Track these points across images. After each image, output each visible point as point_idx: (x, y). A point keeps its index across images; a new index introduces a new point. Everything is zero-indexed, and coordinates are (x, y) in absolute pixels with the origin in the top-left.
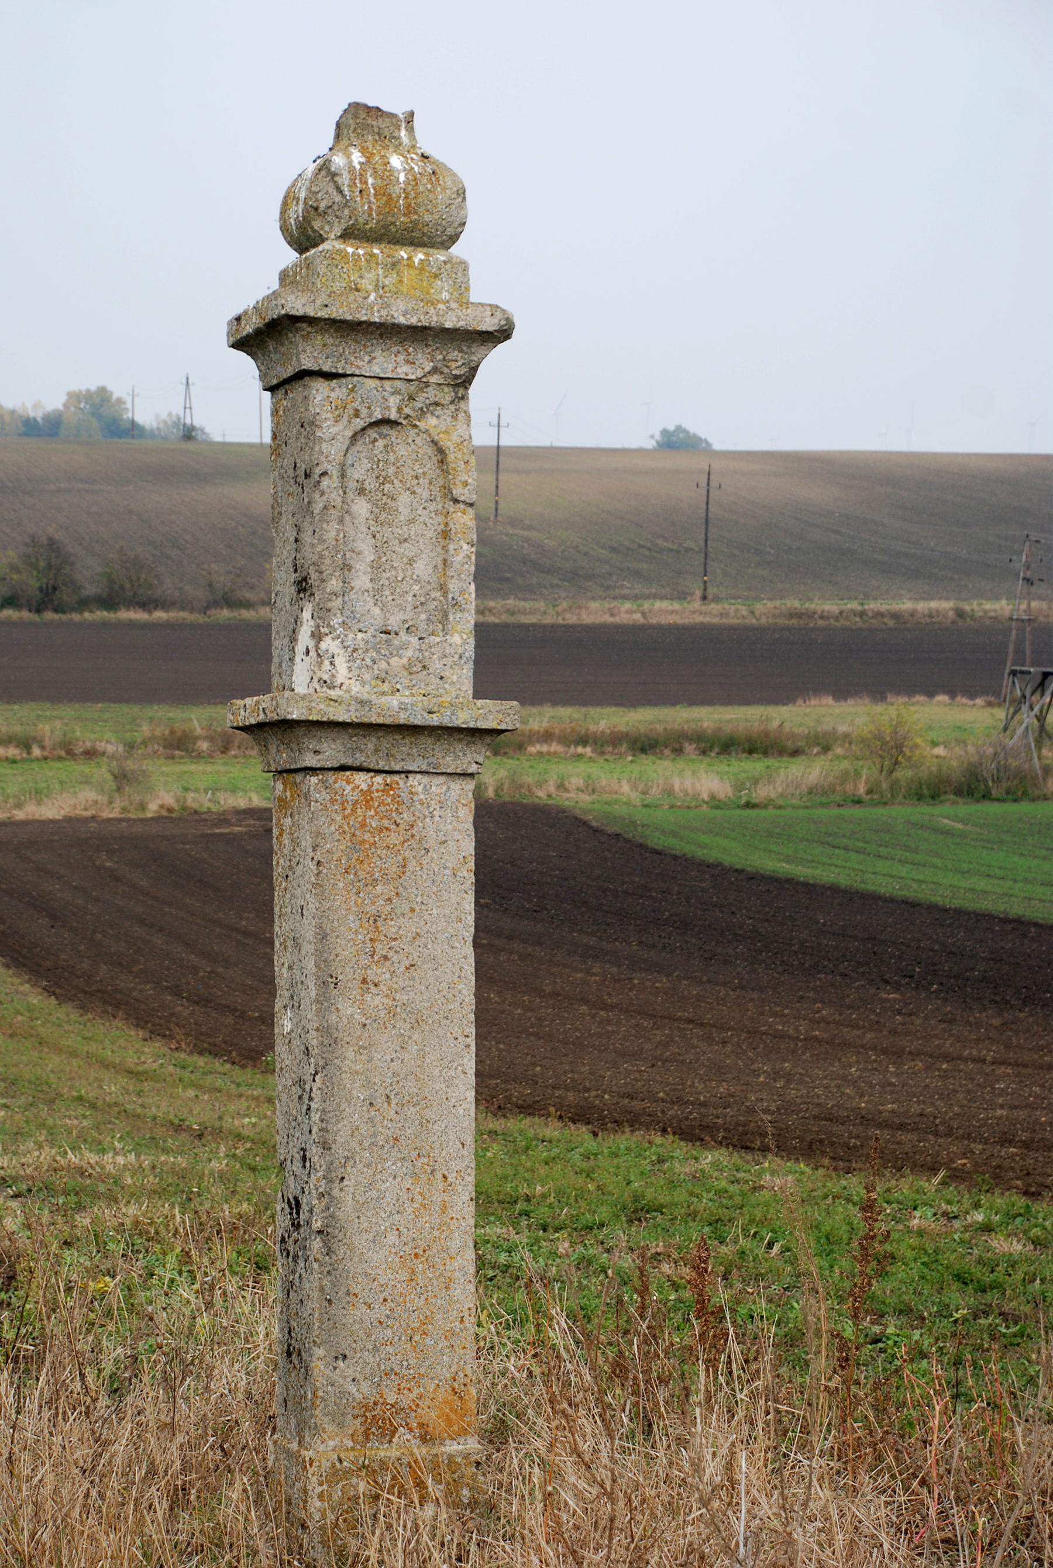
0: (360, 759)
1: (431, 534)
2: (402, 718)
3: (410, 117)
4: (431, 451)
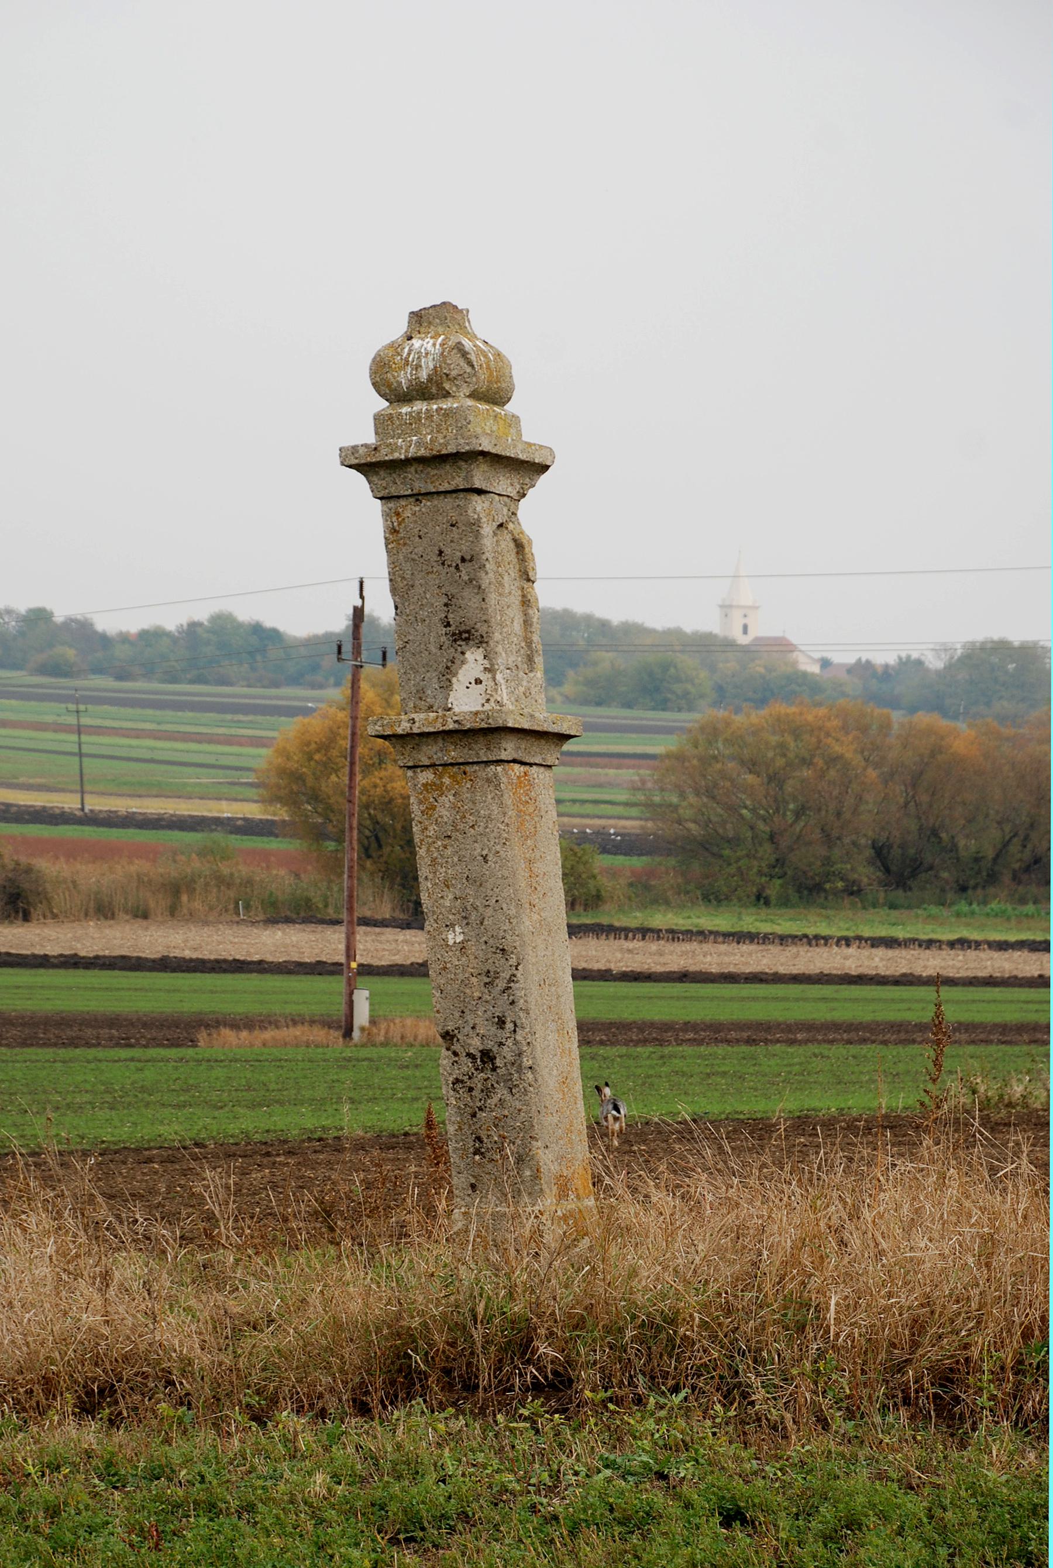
1: (517, 602)
3: (468, 311)
4: (512, 545)
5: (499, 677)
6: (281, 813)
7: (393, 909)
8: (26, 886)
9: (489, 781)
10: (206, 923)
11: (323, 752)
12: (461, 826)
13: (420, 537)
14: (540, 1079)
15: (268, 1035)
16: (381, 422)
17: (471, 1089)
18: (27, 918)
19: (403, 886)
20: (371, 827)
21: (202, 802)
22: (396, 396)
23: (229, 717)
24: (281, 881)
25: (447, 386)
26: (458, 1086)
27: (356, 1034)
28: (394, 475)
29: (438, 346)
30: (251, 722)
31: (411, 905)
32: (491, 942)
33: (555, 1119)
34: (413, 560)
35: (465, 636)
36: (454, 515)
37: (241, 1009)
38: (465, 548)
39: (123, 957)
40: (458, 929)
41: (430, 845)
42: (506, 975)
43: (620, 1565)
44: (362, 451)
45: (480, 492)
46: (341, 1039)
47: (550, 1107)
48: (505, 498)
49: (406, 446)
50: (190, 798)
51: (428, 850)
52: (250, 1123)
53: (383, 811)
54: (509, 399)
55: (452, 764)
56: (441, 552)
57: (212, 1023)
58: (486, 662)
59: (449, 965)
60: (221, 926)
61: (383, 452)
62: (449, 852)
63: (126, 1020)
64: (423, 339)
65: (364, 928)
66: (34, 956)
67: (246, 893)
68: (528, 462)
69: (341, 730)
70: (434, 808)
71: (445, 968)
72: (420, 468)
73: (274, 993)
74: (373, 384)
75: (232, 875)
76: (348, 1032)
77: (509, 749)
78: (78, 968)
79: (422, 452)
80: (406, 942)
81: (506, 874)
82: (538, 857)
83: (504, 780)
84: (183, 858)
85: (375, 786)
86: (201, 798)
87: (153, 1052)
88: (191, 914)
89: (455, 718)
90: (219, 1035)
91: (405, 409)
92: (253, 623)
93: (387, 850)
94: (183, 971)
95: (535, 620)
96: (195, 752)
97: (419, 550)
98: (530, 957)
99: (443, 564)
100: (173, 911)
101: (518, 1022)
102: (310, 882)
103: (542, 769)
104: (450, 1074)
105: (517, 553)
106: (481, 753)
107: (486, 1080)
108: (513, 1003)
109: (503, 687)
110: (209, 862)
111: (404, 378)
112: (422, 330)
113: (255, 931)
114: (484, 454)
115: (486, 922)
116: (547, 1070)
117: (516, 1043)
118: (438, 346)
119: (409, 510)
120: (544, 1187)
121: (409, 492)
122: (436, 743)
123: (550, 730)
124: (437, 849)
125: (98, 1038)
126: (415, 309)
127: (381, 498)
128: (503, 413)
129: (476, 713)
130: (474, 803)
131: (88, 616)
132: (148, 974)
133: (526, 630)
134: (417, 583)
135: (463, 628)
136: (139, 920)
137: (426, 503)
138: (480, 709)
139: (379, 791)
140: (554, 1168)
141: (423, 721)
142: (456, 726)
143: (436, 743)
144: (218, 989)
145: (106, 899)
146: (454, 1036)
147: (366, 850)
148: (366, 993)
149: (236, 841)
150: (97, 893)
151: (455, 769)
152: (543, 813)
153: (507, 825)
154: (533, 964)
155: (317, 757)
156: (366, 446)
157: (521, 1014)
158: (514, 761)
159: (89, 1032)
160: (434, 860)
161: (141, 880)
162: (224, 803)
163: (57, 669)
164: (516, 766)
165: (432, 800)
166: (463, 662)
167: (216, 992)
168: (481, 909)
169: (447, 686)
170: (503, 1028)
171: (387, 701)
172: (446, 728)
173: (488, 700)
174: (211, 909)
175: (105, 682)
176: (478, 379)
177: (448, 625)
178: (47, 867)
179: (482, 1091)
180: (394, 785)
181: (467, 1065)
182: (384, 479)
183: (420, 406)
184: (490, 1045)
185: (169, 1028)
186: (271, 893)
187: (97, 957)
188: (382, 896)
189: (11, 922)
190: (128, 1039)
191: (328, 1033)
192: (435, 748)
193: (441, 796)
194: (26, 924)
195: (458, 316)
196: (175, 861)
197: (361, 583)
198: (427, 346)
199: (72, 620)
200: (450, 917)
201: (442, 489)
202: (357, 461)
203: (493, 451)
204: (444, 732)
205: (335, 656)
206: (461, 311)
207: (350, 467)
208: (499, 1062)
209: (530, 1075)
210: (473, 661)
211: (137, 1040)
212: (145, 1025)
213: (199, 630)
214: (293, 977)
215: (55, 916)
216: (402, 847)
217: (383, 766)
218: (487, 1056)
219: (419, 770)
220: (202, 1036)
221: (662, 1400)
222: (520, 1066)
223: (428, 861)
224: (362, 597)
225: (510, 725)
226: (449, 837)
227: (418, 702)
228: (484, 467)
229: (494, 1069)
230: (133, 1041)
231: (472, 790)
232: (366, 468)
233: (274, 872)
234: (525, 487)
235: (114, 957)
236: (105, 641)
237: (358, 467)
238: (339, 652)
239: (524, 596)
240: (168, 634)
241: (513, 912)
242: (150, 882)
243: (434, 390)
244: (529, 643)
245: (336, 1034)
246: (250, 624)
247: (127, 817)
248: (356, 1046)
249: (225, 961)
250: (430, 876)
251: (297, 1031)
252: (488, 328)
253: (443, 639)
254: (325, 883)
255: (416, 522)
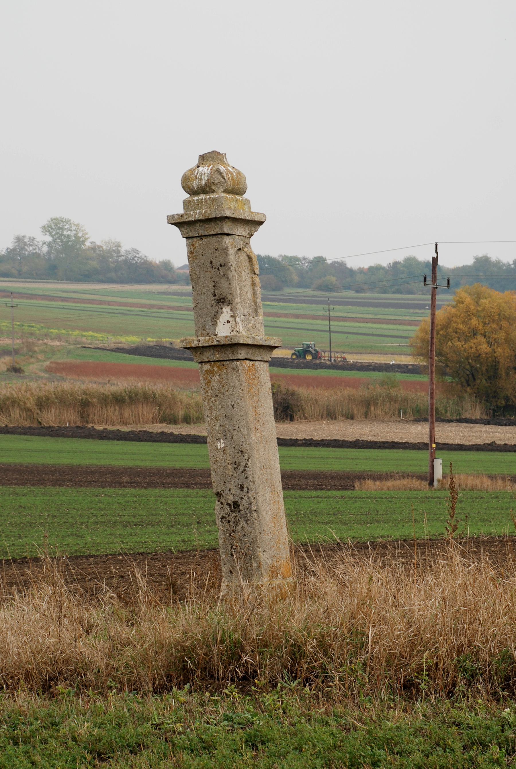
0: (248, 356)
1: (249, 284)
2: (261, 343)
3: (225, 154)
4: (246, 258)
5: (238, 319)
6: (422, 362)
7: (482, 414)
8: (292, 402)
9: (234, 369)
10: (383, 422)
11: (444, 330)
12: (222, 391)
13: (202, 255)
14: (261, 517)
15: (390, 483)
16: (187, 204)
17: (229, 522)
18: (292, 419)
19: (487, 401)
20: (470, 370)
21: (392, 356)
22: (193, 192)
23: (411, 311)
24: (422, 398)
25: (213, 187)
26: (223, 520)
27: (436, 483)
28: (191, 228)
29: (209, 170)
30: (422, 313)
31: (491, 411)
32: (236, 447)
33: (270, 537)
34: (200, 266)
35: (222, 301)
36: (217, 245)
37: (385, 469)
38: (221, 260)
39: (335, 440)
40: (222, 441)
41: (209, 400)
42: (243, 464)
43: (90, 767)
44: (176, 217)
45: (228, 235)
46: (428, 486)
47: (267, 531)
48: (242, 237)
49: (195, 215)
50: (387, 354)
51: (208, 403)
52: (365, 533)
53: (476, 361)
54: (245, 192)
55: (218, 361)
56: (211, 262)
57: (361, 477)
58: (231, 312)
59: (218, 459)
60: (390, 423)
61: (185, 217)
62: (217, 403)
63: (324, 475)
64: (203, 167)
65: (465, 424)
66: (291, 440)
67: (404, 405)
68: (251, 220)
69: (453, 318)
70: (210, 382)
71: (216, 460)
72: (201, 224)
73: (407, 460)
74: (183, 187)
75: (397, 395)
76: (431, 483)
77: (242, 354)
78: (312, 446)
79: (201, 217)
80: (486, 431)
81: (242, 414)
82: (260, 405)
83: (241, 368)
84: (372, 387)
85: (471, 348)
86: (393, 354)
87: (329, 493)
88: (375, 417)
89: (217, 339)
90: (365, 483)
91: (196, 198)
92: (426, 261)
93: (478, 381)
94: (365, 448)
95: (258, 292)
96: (392, 329)
97: (202, 261)
98: (255, 454)
99: (212, 267)
100: (366, 415)
101: (249, 487)
102: (441, 400)
103: (262, 363)
104: (220, 514)
105: (249, 261)
106: (230, 355)
107: (235, 517)
108: (247, 478)
109: (240, 324)
110: (385, 389)
111: (195, 184)
112: (204, 163)
113: (408, 426)
114: (227, 217)
115: (234, 438)
116: (265, 512)
117: (249, 498)
118: (209, 170)
119: (198, 243)
120: (263, 572)
121: (197, 235)
122: (210, 351)
123: (264, 344)
124: (212, 402)
125: (307, 485)
126: (202, 154)
127: (186, 238)
128: (241, 198)
129: (226, 337)
130: (227, 379)
131: (343, 260)
132: (346, 449)
133: (254, 297)
134: (202, 276)
135: (221, 297)
136: (349, 420)
137: (205, 240)
138: (229, 334)
139: (473, 350)
140: (269, 562)
141: (204, 341)
142: (218, 343)
143: (210, 351)
144: (379, 458)
145: (332, 408)
146: (221, 494)
147: (467, 382)
148: (440, 461)
149: (399, 376)
150: (327, 406)
151: (219, 363)
152: (263, 384)
153: (243, 390)
154: (257, 458)
155: (441, 333)
156: (178, 215)
157: (251, 483)
158: (246, 359)
159: (303, 481)
160: (211, 407)
161: (351, 399)
162: (403, 356)
163: (327, 288)
164: (248, 362)
165: (209, 378)
166: (222, 313)
167: (377, 460)
168: (232, 431)
169: (215, 324)
170: (243, 491)
171: (477, 303)
172: (213, 344)
173: (233, 331)
174: (386, 414)
175: (351, 294)
176: (227, 184)
177: (215, 295)
178: (303, 392)
179: (234, 522)
180: (481, 347)
181: (227, 509)
182: (186, 229)
183: (202, 196)
184: (237, 499)
185: (344, 479)
186: (417, 405)
187: (322, 440)
188: (476, 406)
189: (284, 421)
190: (322, 485)
191: (421, 483)
192: (210, 354)
193: (213, 376)
194: (291, 423)
195: (220, 157)
196: (368, 389)
197: (436, 245)
198: (205, 170)
199: (335, 262)
200: (218, 435)
201: (211, 233)
202: (174, 222)
203: (233, 216)
204: (212, 346)
205: (423, 283)
206: (222, 154)
207: (172, 224)
208: (241, 508)
209: (255, 514)
210: (226, 312)
211: (326, 486)
212: (332, 478)
213: (399, 266)
214: (421, 452)
215: (306, 418)
216: (486, 380)
217: (476, 337)
218: (236, 505)
219: (203, 364)
220: (357, 484)
221: (285, 685)
222: (251, 509)
223: (208, 407)
224: (437, 252)
225: (241, 342)
226: (217, 396)
227: (203, 332)
228: (229, 223)
229: (239, 511)
230: (324, 486)
231: (226, 373)
232: (179, 225)
233: (419, 394)
234: (252, 232)
235: (331, 440)
236: (351, 272)
237: (175, 224)
238: (425, 281)
239: (253, 281)
240: (384, 268)
241: (246, 432)
242: (354, 400)
243: (208, 189)
244: (255, 303)
245: (425, 483)
246: (424, 262)
247: (353, 364)
248: (435, 490)
249: (387, 442)
250: (209, 415)
251: (405, 482)
252: (236, 161)
253: (213, 302)
254: (445, 400)
255: (200, 248)
